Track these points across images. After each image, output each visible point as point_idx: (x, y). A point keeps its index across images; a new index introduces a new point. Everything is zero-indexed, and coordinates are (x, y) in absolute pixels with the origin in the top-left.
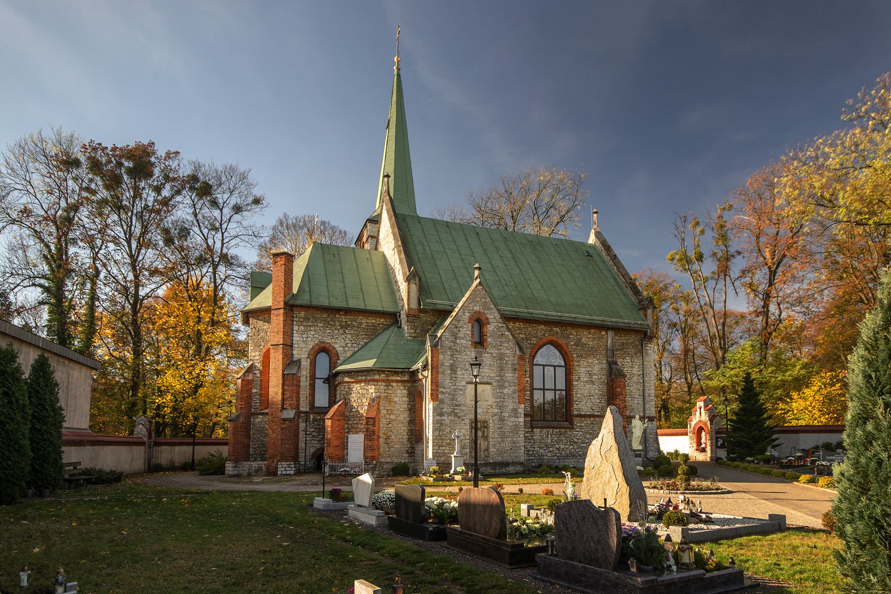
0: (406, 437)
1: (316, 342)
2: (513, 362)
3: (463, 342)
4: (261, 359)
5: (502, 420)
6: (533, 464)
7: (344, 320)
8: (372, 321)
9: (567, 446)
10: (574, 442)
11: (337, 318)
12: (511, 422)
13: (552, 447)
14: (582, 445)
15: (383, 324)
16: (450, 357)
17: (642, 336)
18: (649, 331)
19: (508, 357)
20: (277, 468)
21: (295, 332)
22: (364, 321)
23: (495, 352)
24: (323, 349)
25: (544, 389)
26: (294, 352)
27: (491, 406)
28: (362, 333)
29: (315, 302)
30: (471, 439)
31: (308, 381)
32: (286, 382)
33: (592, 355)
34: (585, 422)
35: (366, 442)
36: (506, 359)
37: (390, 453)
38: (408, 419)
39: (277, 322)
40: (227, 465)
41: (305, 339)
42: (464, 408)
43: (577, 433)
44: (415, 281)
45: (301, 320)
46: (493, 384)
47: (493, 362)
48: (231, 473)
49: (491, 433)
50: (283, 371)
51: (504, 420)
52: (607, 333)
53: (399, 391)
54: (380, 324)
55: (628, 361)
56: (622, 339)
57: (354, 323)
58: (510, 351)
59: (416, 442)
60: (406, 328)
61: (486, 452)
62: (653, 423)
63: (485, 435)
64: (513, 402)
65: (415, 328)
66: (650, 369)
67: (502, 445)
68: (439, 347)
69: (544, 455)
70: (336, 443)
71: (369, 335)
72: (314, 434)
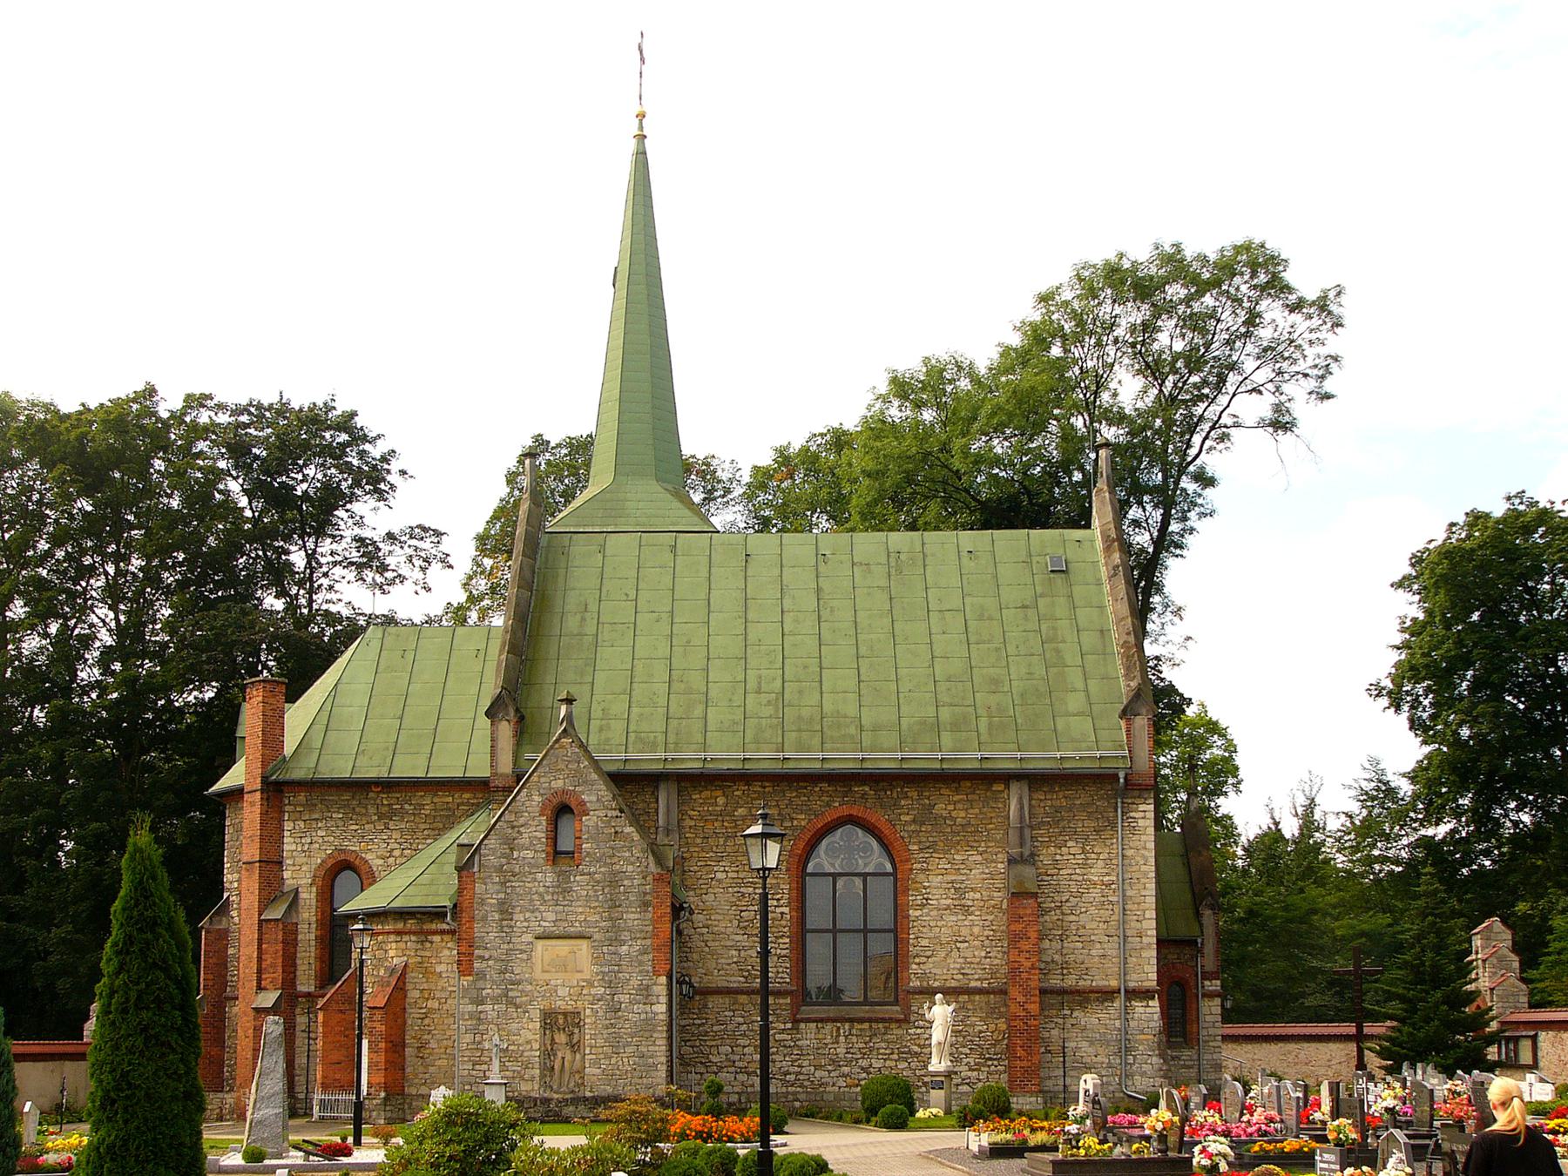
2: (642, 888)
5: (616, 1010)
6: (797, 1104)
9: (888, 1063)
11: (372, 798)
12: (635, 1013)
13: (849, 1063)
15: (468, 804)
19: (631, 879)
21: (286, 834)
22: (428, 801)
23: (600, 870)
25: (835, 931)
26: (286, 875)
28: (423, 826)
33: (963, 843)
36: (626, 882)
37: (427, 1076)
41: (306, 847)
43: (919, 1031)
46: (596, 937)
50: (260, 915)
52: (1008, 787)
53: (447, 952)
55: (1072, 851)
56: (1050, 800)
57: (407, 806)
58: (634, 865)
61: (577, 1076)
62: (1151, 1003)
63: (575, 1041)
66: (1144, 868)
68: (476, 869)
69: (827, 1084)
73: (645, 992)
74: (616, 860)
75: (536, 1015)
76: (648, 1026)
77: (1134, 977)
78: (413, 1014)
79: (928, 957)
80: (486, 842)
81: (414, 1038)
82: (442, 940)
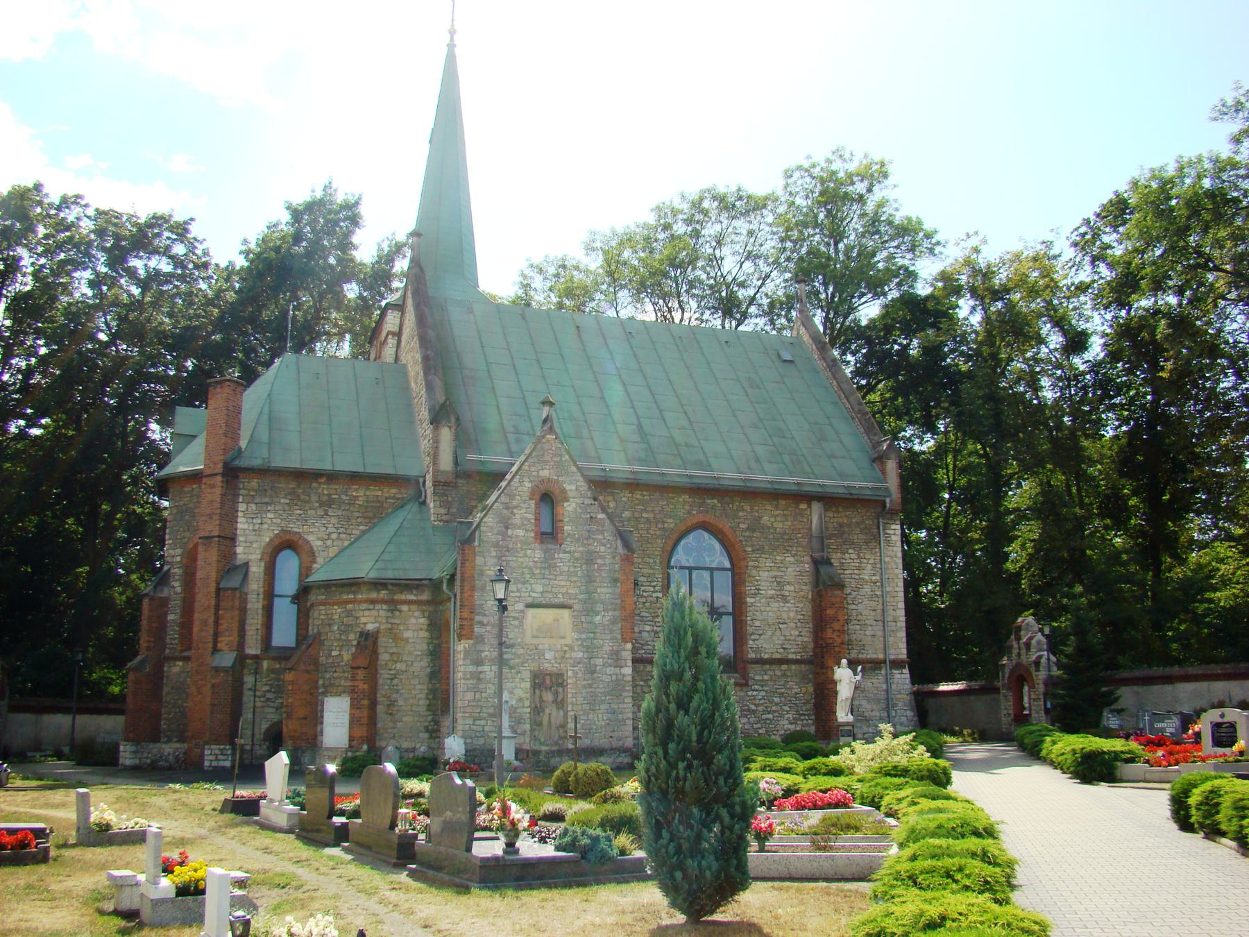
0: (424, 702)
1: (276, 532)
3: (520, 532)
4: (184, 561)
5: (592, 671)
7: (326, 492)
8: (375, 492)
10: (749, 710)
12: (607, 674)
14: (764, 717)
15: (394, 498)
16: (496, 560)
17: (879, 510)
18: (888, 500)
19: (603, 558)
20: (202, 755)
21: (240, 514)
22: (361, 494)
24: (287, 543)
26: (239, 550)
27: (571, 648)
29: (278, 462)
30: (533, 706)
31: (261, 600)
32: (223, 604)
33: (781, 548)
34: (771, 673)
35: (354, 711)
36: (599, 561)
37: (396, 731)
38: (429, 670)
39: (209, 497)
40: (122, 748)
41: (257, 526)
42: (521, 651)
43: (755, 693)
44: (449, 422)
45: (252, 493)
47: (575, 567)
48: (128, 762)
49: (569, 696)
51: (595, 672)
52: (810, 506)
53: (413, 621)
54: (390, 498)
55: (852, 556)
56: (837, 518)
57: (344, 497)
58: (607, 548)
59: (442, 711)
60: (432, 505)
61: (561, 731)
63: (560, 698)
64: (611, 639)
65: (447, 505)
67: (591, 716)
68: (476, 543)
70: (301, 712)
71: (370, 518)
72: (269, 695)
73: (616, 658)
74: (591, 541)
75: (527, 675)
76: (616, 688)
77: (892, 651)
78: (384, 675)
79: (760, 635)
80: (485, 520)
81: (384, 696)
82: (410, 610)
